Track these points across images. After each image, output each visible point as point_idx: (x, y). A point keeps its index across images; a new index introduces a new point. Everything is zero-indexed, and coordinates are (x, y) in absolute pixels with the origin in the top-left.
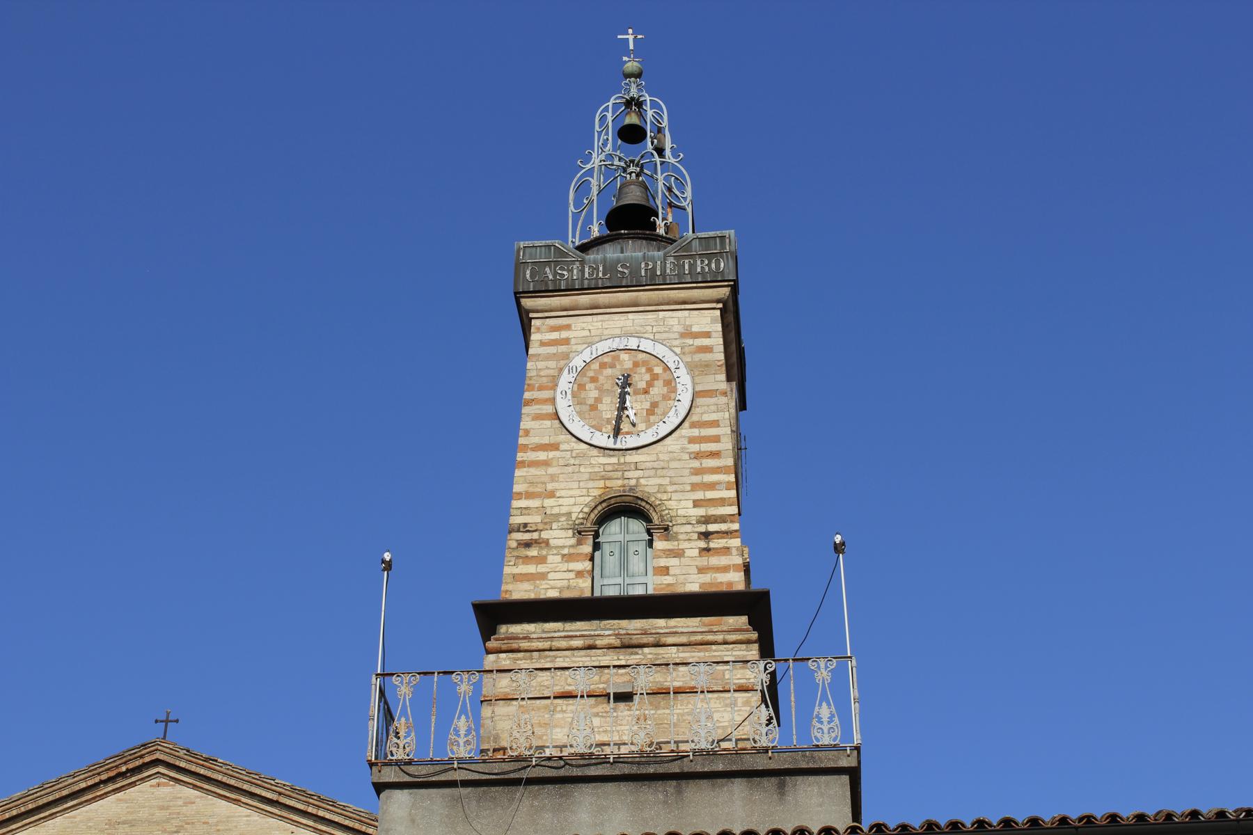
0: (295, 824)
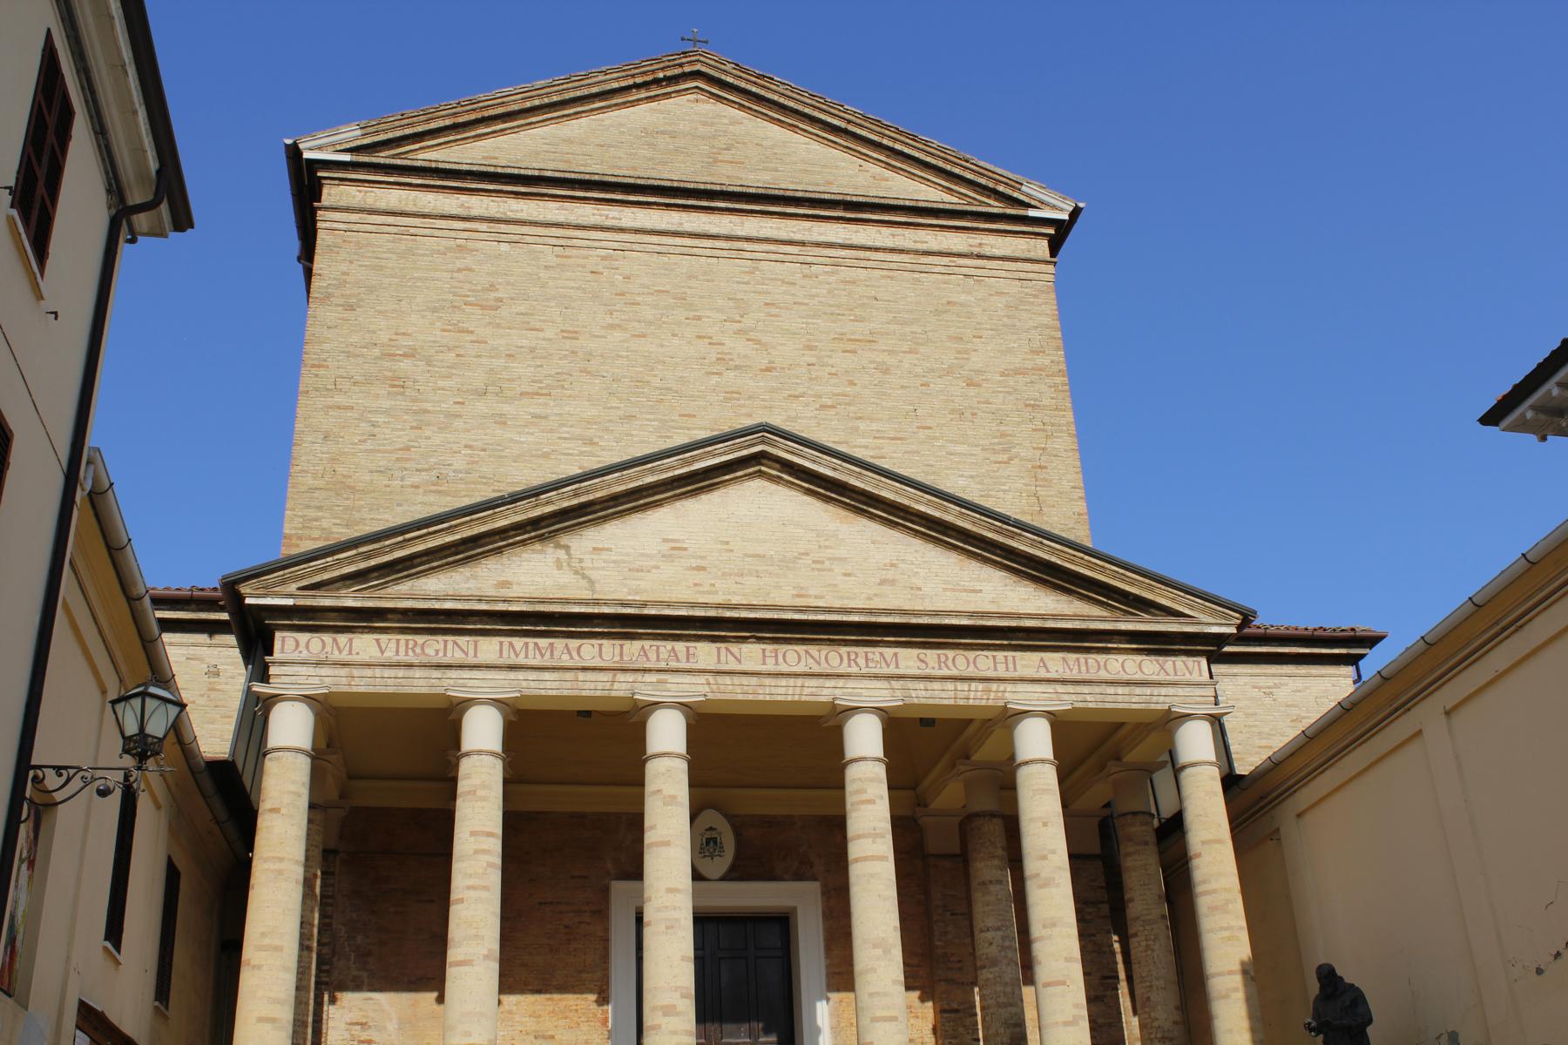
0: (864, 157)
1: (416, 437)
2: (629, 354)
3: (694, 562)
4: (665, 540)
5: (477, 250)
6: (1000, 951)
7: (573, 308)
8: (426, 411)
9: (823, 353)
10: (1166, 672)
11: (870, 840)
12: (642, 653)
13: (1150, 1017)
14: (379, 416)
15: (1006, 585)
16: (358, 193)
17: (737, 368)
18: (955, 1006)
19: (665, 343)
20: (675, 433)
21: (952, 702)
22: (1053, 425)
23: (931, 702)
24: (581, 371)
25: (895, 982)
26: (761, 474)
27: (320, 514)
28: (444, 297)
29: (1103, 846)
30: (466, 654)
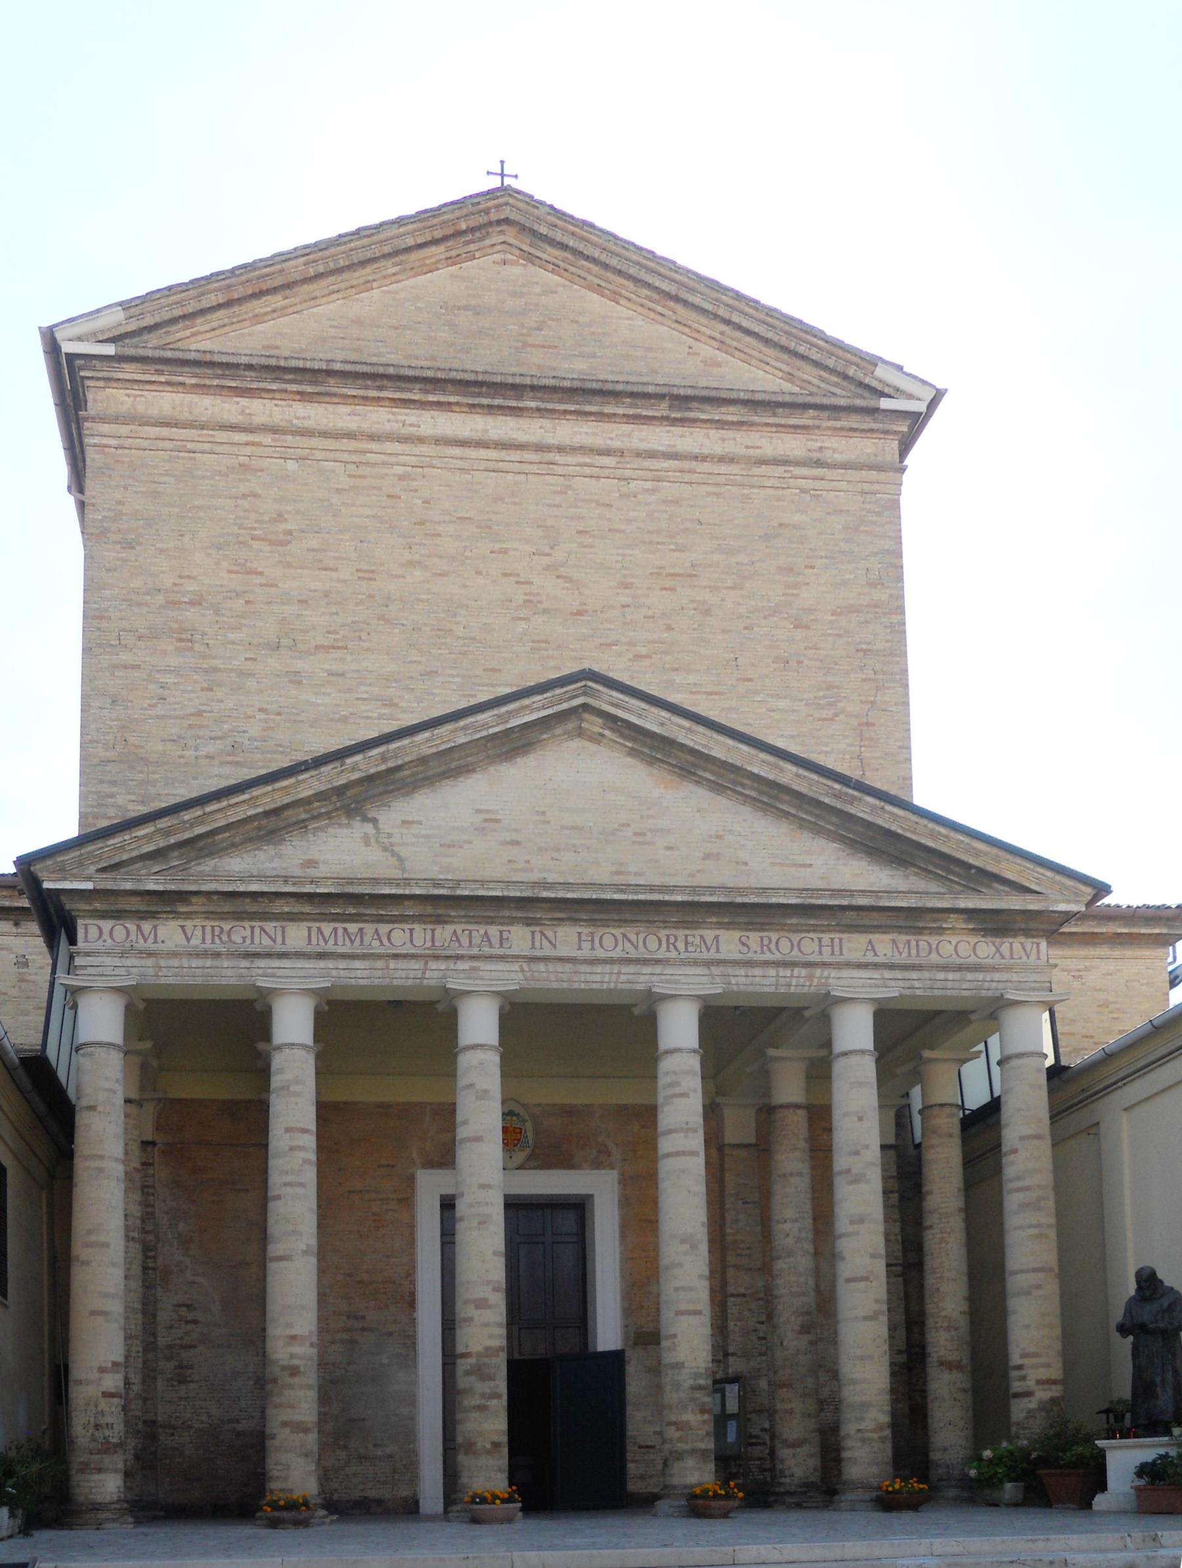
1: (208, 700)
2: (430, 597)
3: (509, 836)
4: (479, 811)
5: (262, 470)
6: (796, 1243)
7: (369, 542)
8: (216, 670)
9: (639, 591)
10: (1001, 955)
11: (682, 1135)
12: (454, 939)
13: (937, 1307)
14: (169, 676)
15: (838, 859)
16: (126, 399)
17: (546, 611)
18: (742, 1291)
19: (468, 584)
20: (478, 690)
21: (772, 989)
22: (884, 673)
23: (751, 989)
24: (378, 619)
25: (700, 1277)
26: (580, 733)
27: (115, 790)
28: (229, 531)
29: (898, 1135)
30: (274, 941)
